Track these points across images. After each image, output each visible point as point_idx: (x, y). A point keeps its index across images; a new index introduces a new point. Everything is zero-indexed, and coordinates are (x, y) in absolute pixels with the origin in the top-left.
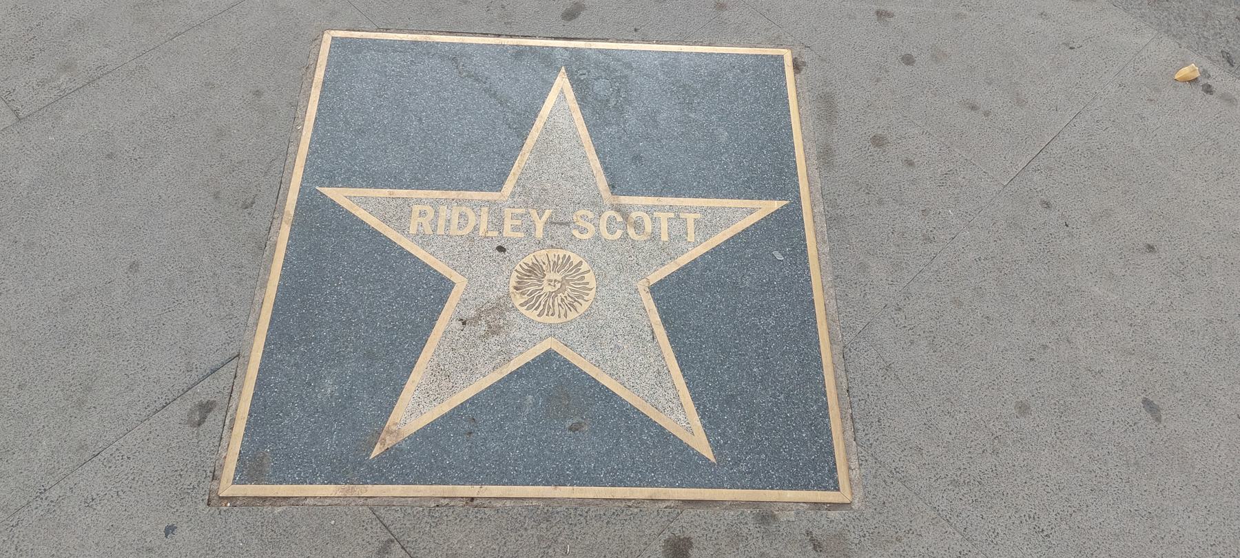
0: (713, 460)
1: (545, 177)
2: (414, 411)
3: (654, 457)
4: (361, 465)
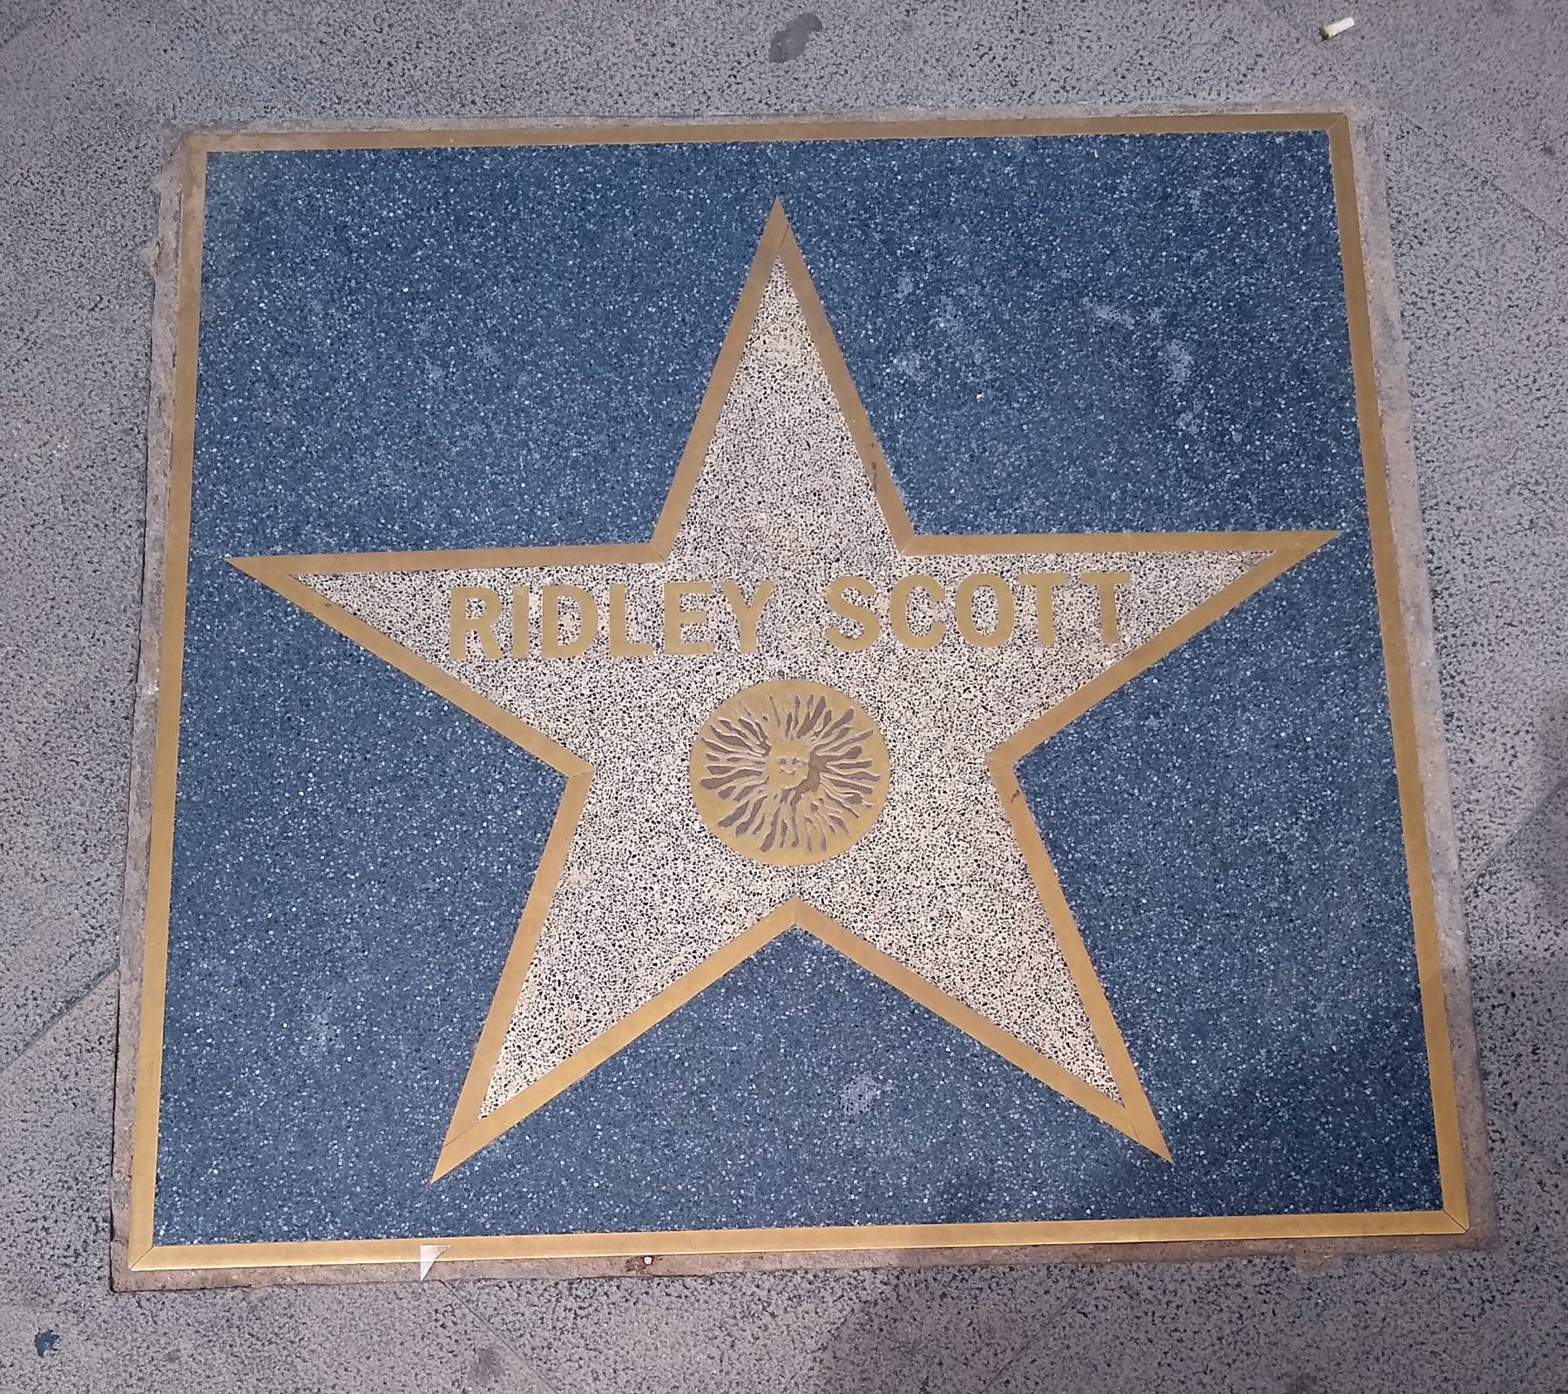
0: (1166, 1156)
1: (752, 496)
2: (514, 1075)
3: (1035, 1156)
4: (414, 1194)
